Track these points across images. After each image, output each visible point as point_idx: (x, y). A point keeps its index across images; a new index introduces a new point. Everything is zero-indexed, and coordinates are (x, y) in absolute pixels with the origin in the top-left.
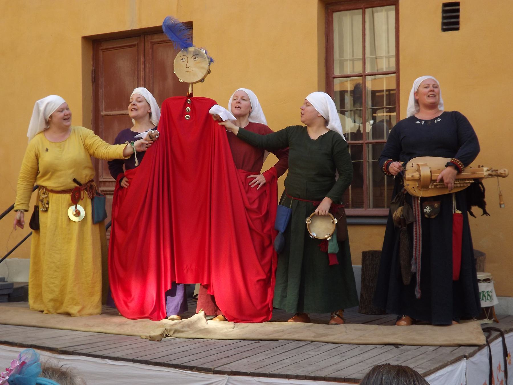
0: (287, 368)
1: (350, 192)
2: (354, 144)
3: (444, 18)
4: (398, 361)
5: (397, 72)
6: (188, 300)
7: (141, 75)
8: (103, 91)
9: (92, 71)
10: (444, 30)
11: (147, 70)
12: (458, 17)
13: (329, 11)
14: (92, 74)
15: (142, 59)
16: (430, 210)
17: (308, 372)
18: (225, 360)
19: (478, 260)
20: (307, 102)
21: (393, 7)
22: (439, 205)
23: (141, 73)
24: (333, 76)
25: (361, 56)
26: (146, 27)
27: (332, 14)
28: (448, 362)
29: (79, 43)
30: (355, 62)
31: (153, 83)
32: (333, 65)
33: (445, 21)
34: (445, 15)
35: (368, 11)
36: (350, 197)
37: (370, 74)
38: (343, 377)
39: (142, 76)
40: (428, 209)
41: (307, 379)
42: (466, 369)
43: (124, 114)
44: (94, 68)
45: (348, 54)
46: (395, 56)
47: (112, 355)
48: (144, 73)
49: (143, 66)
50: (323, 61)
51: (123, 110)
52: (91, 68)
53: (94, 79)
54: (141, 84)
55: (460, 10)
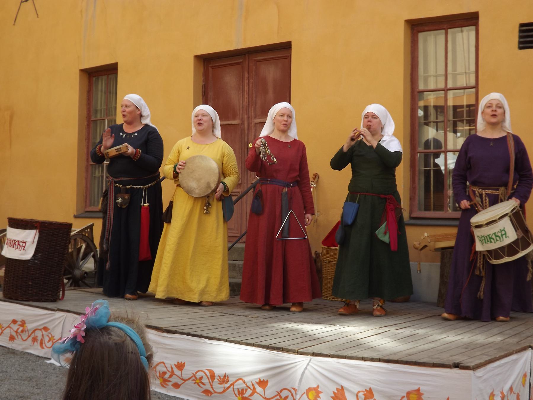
0: (365, 351)
1: (432, 196)
2: (436, 152)
3: (520, 37)
4: (466, 348)
5: (476, 87)
7: (246, 89)
8: (212, 104)
9: (203, 86)
10: (520, 48)
11: (251, 85)
15: (246, 75)
16: (121, 201)
17: (383, 355)
18: (309, 344)
20: (374, 115)
21: (473, 28)
22: (128, 197)
23: (246, 87)
24: (418, 90)
25: (443, 72)
26: (250, 46)
28: (513, 351)
29: (191, 61)
31: (256, 96)
33: (522, 40)
34: (521, 34)
35: (450, 31)
36: (432, 201)
37: (451, 89)
38: (414, 361)
40: (120, 200)
41: (381, 362)
42: (531, 358)
44: (204, 83)
45: (432, 71)
46: (474, 72)
47: (209, 335)
48: (247, 87)
49: (247, 82)
51: (229, 120)
52: (202, 83)
53: (204, 93)
54: (245, 98)
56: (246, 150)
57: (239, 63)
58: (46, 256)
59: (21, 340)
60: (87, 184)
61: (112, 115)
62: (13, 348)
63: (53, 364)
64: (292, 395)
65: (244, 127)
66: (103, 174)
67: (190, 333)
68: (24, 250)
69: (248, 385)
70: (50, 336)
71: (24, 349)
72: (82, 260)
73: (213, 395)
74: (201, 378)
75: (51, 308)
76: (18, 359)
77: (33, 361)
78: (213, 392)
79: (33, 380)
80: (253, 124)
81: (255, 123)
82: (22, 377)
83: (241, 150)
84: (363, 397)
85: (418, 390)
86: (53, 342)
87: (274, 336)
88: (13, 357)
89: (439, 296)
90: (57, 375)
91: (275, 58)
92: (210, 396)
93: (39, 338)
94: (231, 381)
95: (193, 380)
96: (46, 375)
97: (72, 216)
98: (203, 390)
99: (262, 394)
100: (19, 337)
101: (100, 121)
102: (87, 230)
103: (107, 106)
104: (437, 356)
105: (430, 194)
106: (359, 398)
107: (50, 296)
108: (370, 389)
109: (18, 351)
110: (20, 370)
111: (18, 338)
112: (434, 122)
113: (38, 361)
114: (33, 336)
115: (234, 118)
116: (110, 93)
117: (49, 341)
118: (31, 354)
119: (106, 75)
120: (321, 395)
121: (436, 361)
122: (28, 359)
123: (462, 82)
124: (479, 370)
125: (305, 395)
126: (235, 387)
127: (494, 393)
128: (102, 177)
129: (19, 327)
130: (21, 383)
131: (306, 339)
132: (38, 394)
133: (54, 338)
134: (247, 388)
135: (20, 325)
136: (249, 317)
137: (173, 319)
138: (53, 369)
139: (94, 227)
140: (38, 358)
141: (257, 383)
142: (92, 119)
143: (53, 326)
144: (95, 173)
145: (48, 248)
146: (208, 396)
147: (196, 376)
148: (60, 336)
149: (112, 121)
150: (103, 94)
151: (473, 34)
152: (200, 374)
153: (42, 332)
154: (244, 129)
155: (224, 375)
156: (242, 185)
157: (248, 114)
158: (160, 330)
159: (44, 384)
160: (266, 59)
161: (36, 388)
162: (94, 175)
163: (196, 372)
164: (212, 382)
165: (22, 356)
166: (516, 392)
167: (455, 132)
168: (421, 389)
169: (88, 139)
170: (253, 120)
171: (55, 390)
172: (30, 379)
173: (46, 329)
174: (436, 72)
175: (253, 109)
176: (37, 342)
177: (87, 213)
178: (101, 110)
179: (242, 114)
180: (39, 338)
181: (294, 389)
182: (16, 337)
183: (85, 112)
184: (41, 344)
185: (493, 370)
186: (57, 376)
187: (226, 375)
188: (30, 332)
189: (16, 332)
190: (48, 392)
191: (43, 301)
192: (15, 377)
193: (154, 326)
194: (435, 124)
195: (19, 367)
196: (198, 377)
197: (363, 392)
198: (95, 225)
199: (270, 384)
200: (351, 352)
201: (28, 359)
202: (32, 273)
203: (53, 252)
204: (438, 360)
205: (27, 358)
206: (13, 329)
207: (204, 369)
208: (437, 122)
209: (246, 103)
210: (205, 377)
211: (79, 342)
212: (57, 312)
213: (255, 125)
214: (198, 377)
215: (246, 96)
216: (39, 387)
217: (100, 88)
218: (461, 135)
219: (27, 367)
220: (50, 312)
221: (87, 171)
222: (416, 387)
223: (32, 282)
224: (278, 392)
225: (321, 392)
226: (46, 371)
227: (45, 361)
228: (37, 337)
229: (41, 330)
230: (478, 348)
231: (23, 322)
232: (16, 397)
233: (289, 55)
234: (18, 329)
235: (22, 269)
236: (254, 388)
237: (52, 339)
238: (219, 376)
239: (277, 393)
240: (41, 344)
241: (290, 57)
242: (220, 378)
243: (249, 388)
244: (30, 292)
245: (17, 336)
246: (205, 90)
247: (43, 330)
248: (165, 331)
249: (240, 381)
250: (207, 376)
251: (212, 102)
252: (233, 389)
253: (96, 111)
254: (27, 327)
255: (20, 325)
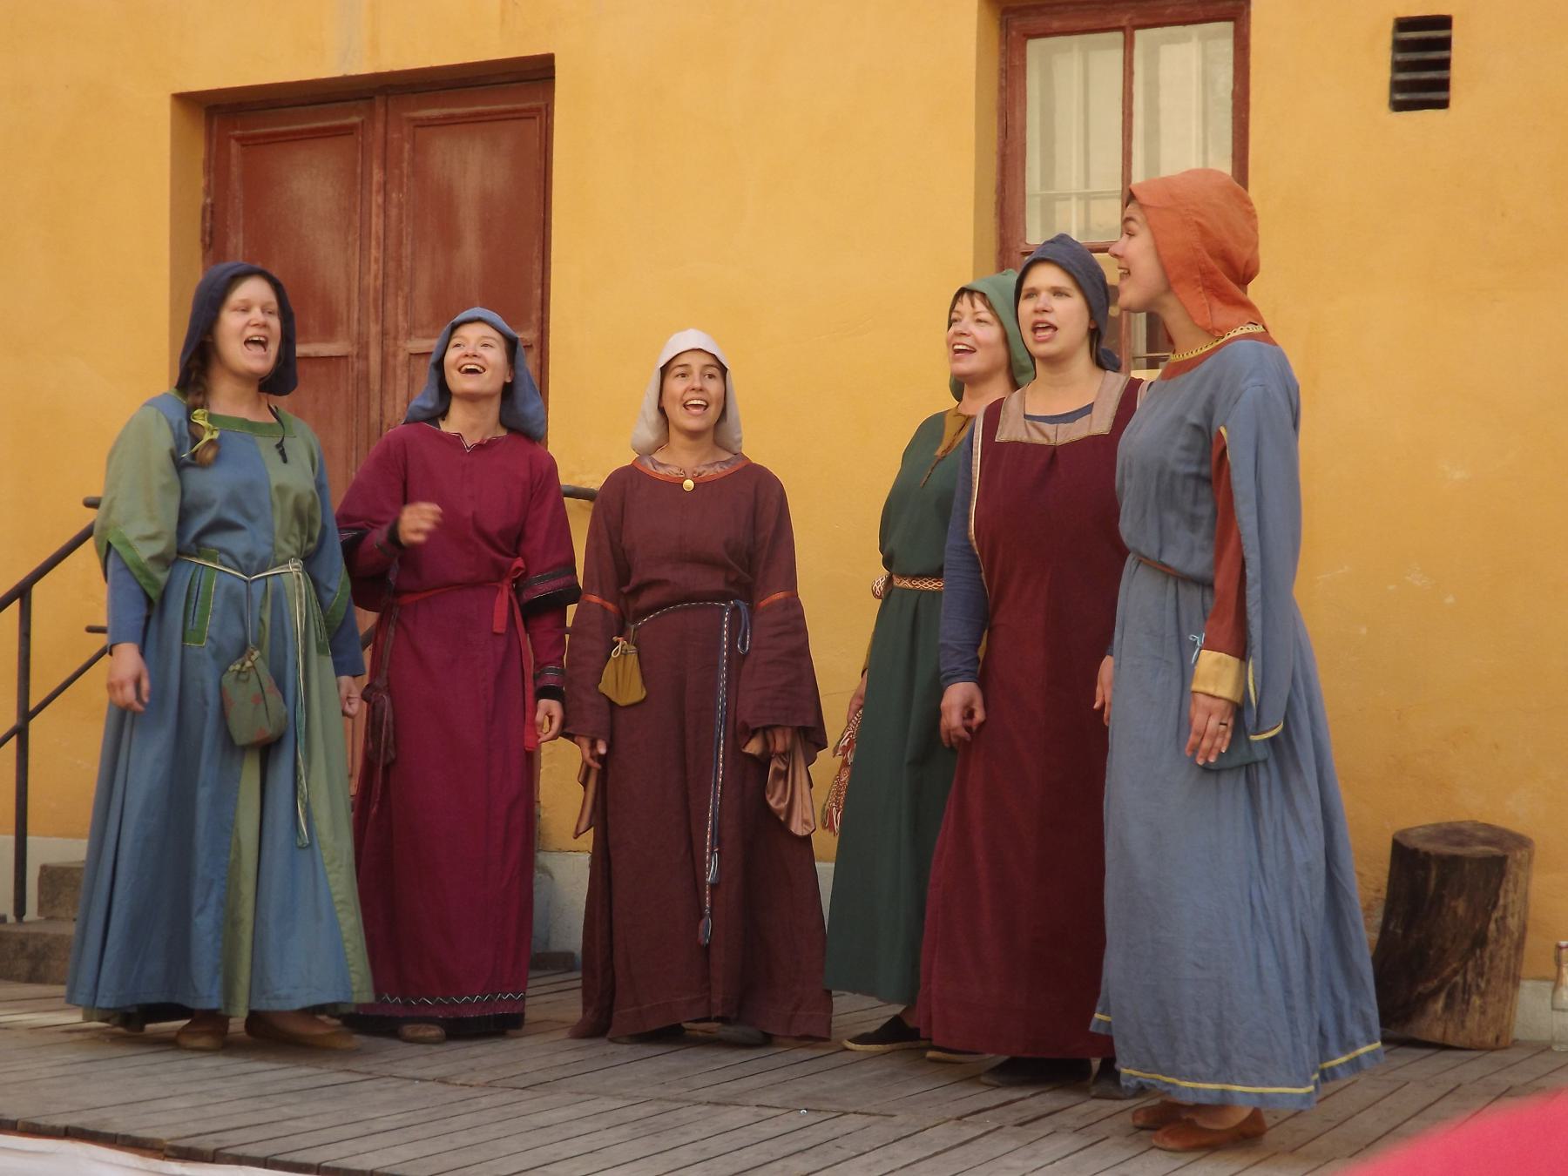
3: (1398, 67)
6: (531, 979)
10: (1398, 106)
11: (394, 212)
12: (1445, 64)
13: (1014, 33)
14: (204, 218)
15: (377, 175)
19: (1509, 861)
21: (1228, 27)
24: (1023, 248)
26: (396, 68)
27: (1024, 45)
29: (164, 112)
30: (1093, 203)
32: (1023, 210)
33: (1403, 76)
34: (1400, 57)
35: (1140, 36)
39: (377, 232)
43: (313, 354)
44: (209, 201)
45: (1070, 177)
46: (1119, 194)
49: (380, 200)
50: (991, 197)
52: (199, 199)
54: (372, 259)
55: (1453, 40)
57: (348, 130)
67: (275, 1157)
80: (402, 356)
81: (411, 354)
83: (354, 454)
136: (456, 1085)
137: (183, 1105)
151: (1226, 47)
158: (151, 1149)
160: (452, 116)
170: (400, 343)
179: (359, 320)
193: (125, 1137)
209: (376, 277)
213: (409, 359)
215: (374, 252)
246: (211, 227)
248: (171, 1153)
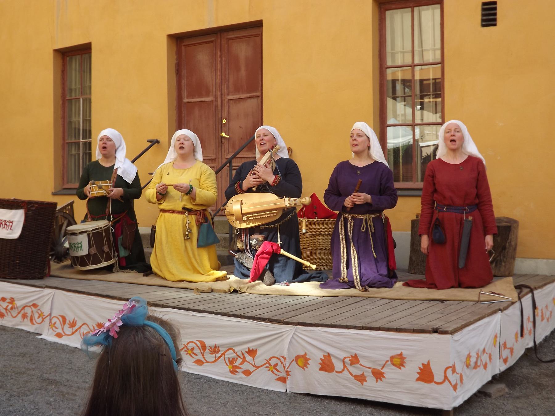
1: (401, 167)
3: (483, 15)
4: (442, 314)
5: (442, 62)
7: (218, 68)
9: (176, 64)
10: (483, 26)
11: (223, 63)
15: (219, 53)
18: (293, 313)
21: (438, 6)
23: (218, 65)
24: (386, 66)
29: (164, 41)
31: (228, 73)
33: (484, 18)
34: (484, 13)
35: (416, 9)
37: (418, 64)
44: (177, 62)
46: (440, 49)
48: (220, 65)
49: (220, 60)
51: (202, 97)
52: (174, 62)
56: (220, 126)
58: (33, 235)
59: (11, 316)
60: (63, 162)
61: (87, 94)
62: (3, 325)
63: (44, 339)
64: (282, 363)
65: (218, 103)
66: (80, 151)
68: (11, 229)
69: (238, 354)
70: (40, 313)
71: (14, 325)
72: (64, 237)
73: (205, 364)
74: (193, 349)
75: (40, 285)
76: (10, 336)
77: (24, 337)
78: (205, 362)
79: (27, 356)
81: (229, 100)
82: (15, 353)
84: (349, 362)
85: (401, 354)
86: (42, 318)
87: (259, 307)
88: (4, 333)
89: (410, 263)
90: (49, 350)
91: (247, 36)
92: (202, 365)
93: (29, 315)
94: (222, 351)
95: (185, 351)
96: (38, 350)
97: (50, 193)
98: (195, 360)
99: (252, 362)
100: (9, 314)
101: (75, 100)
102: (67, 208)
103: (81, 85)
104: (416, 322)
105: (399, 166)
106: (345, 363)
107: (37, 273)
108: (356, 354)
109: (8, 327)
110: (13, 347)
111: (8, 315)
112: (402, 97)
113: (29, 337)
114: (22, 312)
115: (207, 95)
116: (84, 72)
117: (39, 317)
118: (22, 330)
119: (80, 54)
120: (309, 362)
121: (416, 327)
122: (19, 335)
123: (430, 57)
124: (456, 334)
125: (294, 362)
126: (226, 356)
127: (471, 355)
128: (79, 155)
129: (8, 304)
130: (15, 359)
131: (290, 309)
132: (34, 369)
133: (44, 314)
134: (237, 357)
135: (9, 303)
138: (44, 344)
139: (74, 205)
140: (28, 334)
141: (246, 352)
142: (67, 98)
143: (42, 302)
144: (71, 150)
145: (34, 227)
146: (200, 365)
147: (188, 347)
148: (49, 313)
149: (86, 100)
150: (77, 73)
151: (438, 12)
152: (191, 345)
153: (31, 309)
154: (218, 106)
155: (214, 346)
156: (217, 160)
157: (221, 91)
159: (38, 359)
161: (31, 363)
162: (70, 153)
163: (188, 344)
164: (204, 352)
165: (13, 333)
166: (488, 352)
167: (395, 99)
168: (403, 353)
169: (63, 117)
170: (226, 97)
171: (49, 365)
172: (23, 355)
173: (35, 305)
174: (403, 49)
175: (226, 86)
176: (27, 318)
177: (65, 190)
178: (76, 89)
180: (29, 315)
181: (283, 357)
182: (6, 314)
183: (60, 91)
184: (31, 320)
185: (468, 334)
186: (49, 351)
187: (217, 346)
188: (20, 309)
189: (6, 309)
190: (42, 367)
191: (30, 279)
192: (9, 353)
194: (403, 98)
195: (11, 343)
196: (190, 348)
197: (349, 357)
198: (75, 202)
199: (259, 353)
200: (335, 321)
201: (19, 335)
202: (19, 251)
203: (39, 231)
204: (418, 325)
205: (18, 334)
206: (2, 307)
207: (194, 340)
208: (404, 97)
209: (219, 80)
210: (196, 348)
211: (113, 337)
212: (45, 289)
214: (190, 348)
215: (219, 73)
216: (33, 363)
217: (74, 67)
218: (420, 108)
219: (18, 343)
220: (38, 289)
221: (63, 149)
222: (399, 352)
223: (19, 261)
224: (267, 360)
225: (310, 359)
226: (38, 346)
227: (36, 337)
228: (27, 313)
229: (30, 306)
230: (453, 313)
231: (12, 299)
232: (13, 373)
233: (260, 33)
234: (7, 306)
235: (9, 248)
236: (244, 357)
237: (42, 315)
238: (210, 347)
239: (266, 361)
240: (31, 320)
241: (261, 35)
242: (211, 349)
243: (239, 357)
244: (18, 270)
245: (7, 313)
247: (32, 307)
249: (231, 351)
250: (198, 347)
251: (185, 79)
252: (224, 358)
253: (71, 90)
254: (16, 304)
255: (9, 303)
